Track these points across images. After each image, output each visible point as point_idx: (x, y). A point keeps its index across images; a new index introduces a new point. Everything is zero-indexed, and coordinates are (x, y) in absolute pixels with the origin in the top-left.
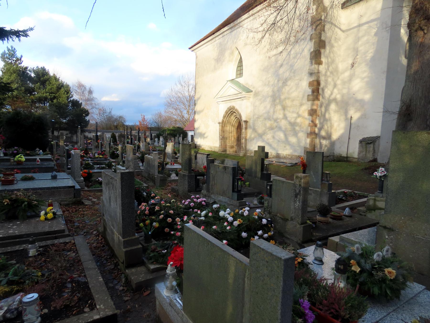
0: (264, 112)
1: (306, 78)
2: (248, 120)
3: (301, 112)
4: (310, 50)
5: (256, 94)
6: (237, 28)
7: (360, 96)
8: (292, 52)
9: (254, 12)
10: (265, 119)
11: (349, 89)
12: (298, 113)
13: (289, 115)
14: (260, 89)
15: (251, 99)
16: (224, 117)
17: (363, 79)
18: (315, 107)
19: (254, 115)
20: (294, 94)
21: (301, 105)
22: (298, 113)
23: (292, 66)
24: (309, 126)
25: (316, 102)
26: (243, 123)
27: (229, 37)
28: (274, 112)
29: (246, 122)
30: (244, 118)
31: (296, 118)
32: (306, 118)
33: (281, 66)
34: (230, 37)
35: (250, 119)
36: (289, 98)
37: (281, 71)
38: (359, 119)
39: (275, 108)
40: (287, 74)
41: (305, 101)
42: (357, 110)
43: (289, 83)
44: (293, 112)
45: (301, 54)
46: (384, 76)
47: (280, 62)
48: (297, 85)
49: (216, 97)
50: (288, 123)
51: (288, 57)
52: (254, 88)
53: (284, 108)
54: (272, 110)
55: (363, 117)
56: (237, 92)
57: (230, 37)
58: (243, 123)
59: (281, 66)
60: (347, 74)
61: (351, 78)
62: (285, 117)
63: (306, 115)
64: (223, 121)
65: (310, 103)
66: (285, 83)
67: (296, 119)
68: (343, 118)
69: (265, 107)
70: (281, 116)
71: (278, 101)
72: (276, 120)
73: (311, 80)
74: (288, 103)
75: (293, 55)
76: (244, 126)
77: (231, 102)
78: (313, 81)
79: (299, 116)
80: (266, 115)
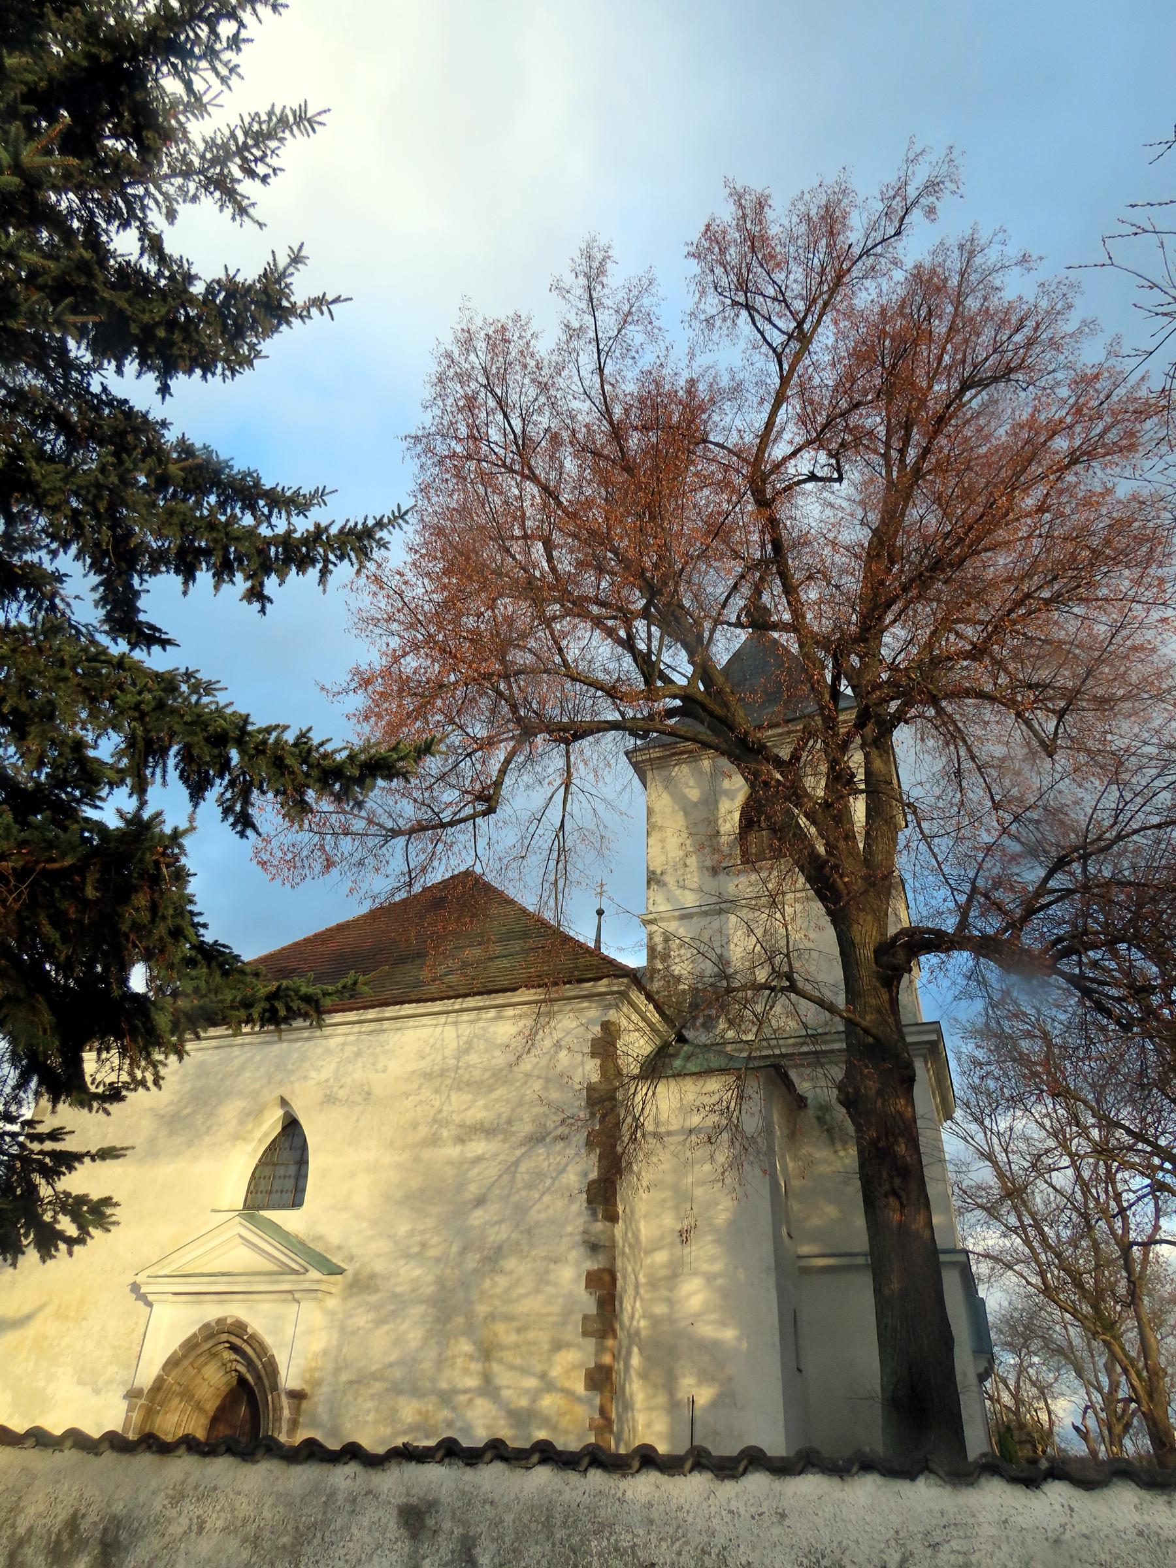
0: (394, 1356)
1: (573, 1255)
2: (307, 1388)
3: (555, 1372)
4: (586, 1175)
5: (362, 1284)
6: (298, 1040)
7: (707, 1330)
8: (523, 1168)
9: (424, 1033)
10: (396, 1389)
11: (670, 1302)
12: (543, 1376)
13: (503, 1377)
14: (379, 1266)
15: (331, 1303)
16: (172, 1363)
17: (710, 1278)
18: (607, 1359)
19: (337, 1371)
20: (530, 1305)
21: (558, 1346)
22: (543, 1376)
23: (521, 1210)
24: (590, 1428)
25: (610, 1342)
26: (285, 1402)
27: (252, 1057)
28: (440, 1363)
29: (297, 1396)
30: (290, 1377)
31: (536, 1395)
32: (579, 1399)
33: (480, 1201)
34: (258, 1058)
35: (317, 1384)
36: (508, 1318)
37: (477, 1217)
38: (714, 1405)
39: (447, 1346)
40: (500, 1234)
41: (572, 1331)
42: (704, 1377)
43: (510, 1263)
44: (525, 1371)
45: (554, 1179)
46: (771, 1281)
47: (473, 1190)
48: (542, 1279)
49: (148, 1272)
50: (503, 1414)
51: (506, 1178)
52: (351, 1258)
53: (487, 1352)
54: (432, 1353)
55: (726, 1400)
56: (270, 1266)
57: (258, 1058)
58: (285, 1402)
59: (480, 1201)
60: (661, 1257)
61: (675, 1273)
62: (489, 1388)
63: (579, 1387)
64: (158, 1385)
65: (590, 1344)
66: (493, 1258)
67: (534, 1401)
68: (662, 1399)
69: (398, 1341)
70: (472, 1382)
71: (460, 1320)
72: (446, 1398)
73: (596, 1267)
74: (505, 1334)
75: (526, 1176)
76: (286, 1413)
77: (201, 1302)
78: (600, 1271)
79: (549, 1385)
80: (398, 1374)
